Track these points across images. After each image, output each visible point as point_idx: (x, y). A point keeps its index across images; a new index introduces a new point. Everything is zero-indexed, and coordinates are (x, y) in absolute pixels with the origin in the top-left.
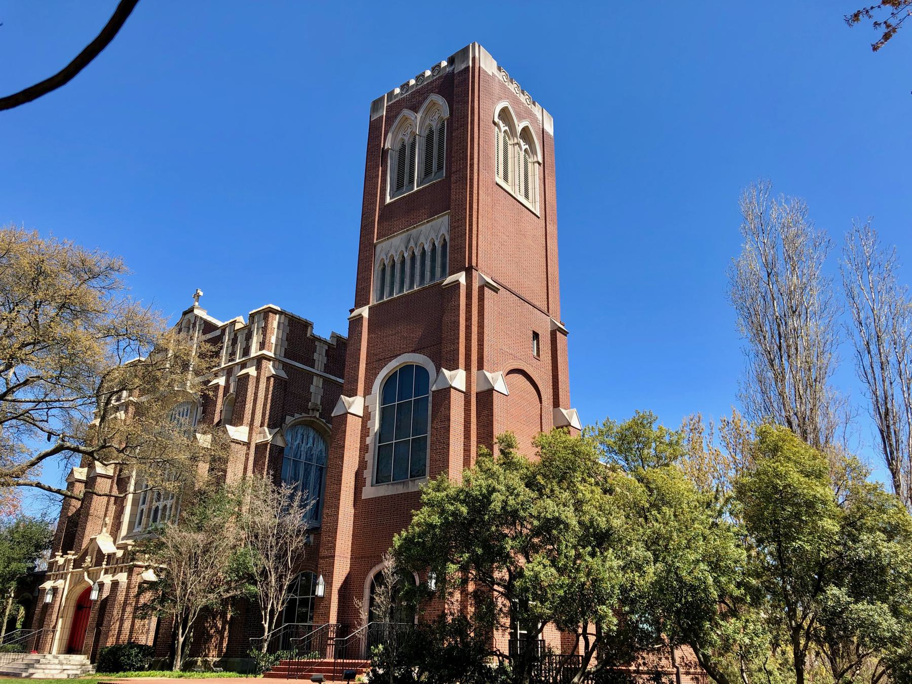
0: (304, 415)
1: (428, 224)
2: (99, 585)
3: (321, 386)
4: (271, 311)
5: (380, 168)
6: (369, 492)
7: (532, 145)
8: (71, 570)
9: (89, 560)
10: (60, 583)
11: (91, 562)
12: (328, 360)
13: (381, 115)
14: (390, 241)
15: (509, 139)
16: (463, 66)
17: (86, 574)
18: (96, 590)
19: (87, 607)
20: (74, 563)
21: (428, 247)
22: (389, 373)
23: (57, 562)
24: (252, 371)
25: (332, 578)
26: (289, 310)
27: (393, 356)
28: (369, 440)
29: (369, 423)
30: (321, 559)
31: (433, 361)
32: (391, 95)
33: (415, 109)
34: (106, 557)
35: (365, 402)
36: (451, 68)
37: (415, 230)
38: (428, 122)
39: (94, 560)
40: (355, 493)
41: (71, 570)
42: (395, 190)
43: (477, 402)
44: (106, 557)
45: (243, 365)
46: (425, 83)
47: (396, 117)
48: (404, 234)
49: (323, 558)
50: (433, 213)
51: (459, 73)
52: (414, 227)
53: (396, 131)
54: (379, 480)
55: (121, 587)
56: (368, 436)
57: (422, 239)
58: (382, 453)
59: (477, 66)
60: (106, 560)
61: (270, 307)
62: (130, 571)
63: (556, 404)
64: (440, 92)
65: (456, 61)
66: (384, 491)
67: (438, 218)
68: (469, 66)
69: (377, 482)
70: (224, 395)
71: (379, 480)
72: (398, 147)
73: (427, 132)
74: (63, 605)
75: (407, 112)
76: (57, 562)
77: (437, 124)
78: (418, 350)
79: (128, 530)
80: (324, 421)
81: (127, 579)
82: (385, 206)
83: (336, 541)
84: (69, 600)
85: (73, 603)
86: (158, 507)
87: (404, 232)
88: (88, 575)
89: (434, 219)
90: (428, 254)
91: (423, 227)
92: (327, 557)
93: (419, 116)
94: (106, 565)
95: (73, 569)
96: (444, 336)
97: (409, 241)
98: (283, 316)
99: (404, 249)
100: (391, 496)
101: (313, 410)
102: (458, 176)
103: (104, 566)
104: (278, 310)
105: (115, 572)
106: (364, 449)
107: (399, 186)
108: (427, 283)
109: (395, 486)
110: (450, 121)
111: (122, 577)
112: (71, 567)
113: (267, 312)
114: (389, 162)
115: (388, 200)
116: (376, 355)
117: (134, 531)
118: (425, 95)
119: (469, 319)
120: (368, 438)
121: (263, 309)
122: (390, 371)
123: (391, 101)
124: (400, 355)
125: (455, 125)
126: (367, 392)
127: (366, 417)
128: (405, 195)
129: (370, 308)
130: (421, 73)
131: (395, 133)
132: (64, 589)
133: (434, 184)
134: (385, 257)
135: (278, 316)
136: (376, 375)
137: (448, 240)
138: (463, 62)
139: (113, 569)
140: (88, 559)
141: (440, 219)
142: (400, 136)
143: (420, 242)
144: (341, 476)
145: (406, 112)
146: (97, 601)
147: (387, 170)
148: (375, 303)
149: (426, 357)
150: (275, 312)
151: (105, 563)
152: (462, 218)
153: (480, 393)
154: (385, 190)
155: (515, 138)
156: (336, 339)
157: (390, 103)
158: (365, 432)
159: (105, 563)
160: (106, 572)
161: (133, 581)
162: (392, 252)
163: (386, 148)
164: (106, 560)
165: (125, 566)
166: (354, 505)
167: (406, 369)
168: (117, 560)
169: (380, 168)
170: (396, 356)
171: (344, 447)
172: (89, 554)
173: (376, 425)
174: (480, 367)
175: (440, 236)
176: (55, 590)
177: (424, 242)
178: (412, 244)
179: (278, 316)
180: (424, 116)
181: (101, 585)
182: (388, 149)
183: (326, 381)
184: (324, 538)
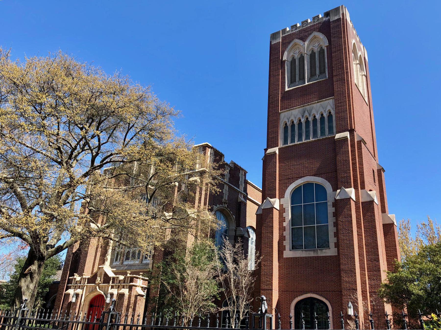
0: (221, 205)
1: (318, 104)
2: (110, 294)
3: (227, 190)
4: (207, 146)
5: (280, 71)
6: (288, 254)
7: (362, 66)
8: (86, 284)
9: (99, 279)
10: (79, 291)
11: (100, 281)
12: (230, 176)
13: (278, 41)
14: (291, 111)
15: (354, 61)
16: (336, 18)
17: (97, 287)
18: (109, 297)
19: (96, 306)
20: (88, 280)
21: (318, 117)
22: (296, 187)
23: (75, 279)
24: (197, 178)
25: (272, 302)
26: (215, 147)
27: (299, 177)
28: (285, 224)
29: (284, 215)
30: (262, 290)
31: (329, 182)
32: (284, 31)
33: (303, 39)
34: (112, 279)
35: (280, 202)
36: (327, 19)
37: (308, 106)
38: (311, 47)
39: (102, 280)
40: (278, 254)
41: (86, 284)
42: (290, 83)
43: (246, 210)
44: (112, 279)
45: (190, 176)
46: (309, 26)
47: (289, 43)
48: (301, 108)
49: (264, 290)
50: (321, 97)
51: (333, 21)
52: (308, 105)
53: (290, 50)
54: (294, 247)
55: (126, 297)
56: (285, 222)
57: (314, 112)
58: (295, 233)
59: (345, 18)
60: (111, 280)
61: (207, 144)
62: (130, 288)
63: (383, 210)
64: (320, 31)
65: (331, 14)
66: (299, 254)
67: (325, 100)
68: (341, 18)
69: (293, 249)
70: (178, 191)
71: (294, 247)
72: (290, 60)
73: (310, 52)
74: (83, 304)
75: (298, 41)
76: (75, 279)
77: (318, 48)
78: (317, 175)
79: (110, 263)
80: (229, 209)
81: (129, 293)
82: (285, 92)
83: (272, 281)
84: (86, 301)
85: (87, 303)
86: (129, 251)
87: (301, 107)
88: (99, 288)
89: (323, 101)
90: (319, 121)
91: (314, 105)
92: (266, 290)
93: (306, 43)
94: (112, 283)
95: (87, 284)
96: (338, 168)
97: (304, 112)
98: (212, 150)
99: (301, 117)
100: (306, 258)
101: (225, 203)
102: (338, 78)
103: (111, 284)
104: (210, 146)
105: (75, 288)
106: (282, 229)
107: (292, 81)
108: (319, 137)
109: (308, 252)
110: (329, 48)
111: (125, 291)
112: (86, 282)
113: (207, 146)
114: (286, 67)
115: (287, 89)
116: (286, 176)
117: (113, 264)
118: (310, 32)
119: (354, 159)
120: (284, 223)
121: (203, 145)
122: (297, 186)
123: (285, 34)
124: (304, 177)
125: (333, 50)
126: (282, 196)
127: (282, 210)
128: (300, 86)
129: (279, 149)
130: (305, 20)
131: (289, 52)
132: (82, 295)
133: (320, 81)
134: (287, 120)
135: (210, 149)
136: (287, 187)
137: (333, 112)
138: (336, 15)
139: (117, 286)
140: (99, 279)
141: (327, 101)
142: (292, 54)
143: (313, 113)
144: (273, 243)
145: (297, 41)
146: (110, 304)
147: (285, 72)
148: (282, 146)
149: (324, 179)
150: (209, 147)
151: (111, 282)
152: (343, 101)
153: (364, 202)
154: (285, 83)
155: (357, 61)
156: (233, 165)
157: (284, 35)
158: (282, 219)
159: (111, 282)
160: (112, 287)
161: (132, 294)
162: (292, 118)
163: (284, 59)
164: (111, 280)
165: (116, 285)
166: (278, 260)
167: (308, 185)
168: (77, 282)
169: (280, 71)
170: (301, 177)
171: (273, 227)
172: (98, 276)
173: (288, 216)
174: (363, 187)
175: (327, 111)
176: (77, 295)
177: (315, 113)
178: (306, 114)
179: (210, 149)
180: (309, 43)
181: (112, 295)
182: (285, 61)
183: (230, 187)
184: (263, 279)
